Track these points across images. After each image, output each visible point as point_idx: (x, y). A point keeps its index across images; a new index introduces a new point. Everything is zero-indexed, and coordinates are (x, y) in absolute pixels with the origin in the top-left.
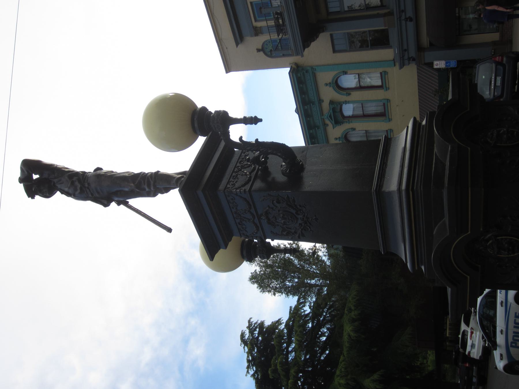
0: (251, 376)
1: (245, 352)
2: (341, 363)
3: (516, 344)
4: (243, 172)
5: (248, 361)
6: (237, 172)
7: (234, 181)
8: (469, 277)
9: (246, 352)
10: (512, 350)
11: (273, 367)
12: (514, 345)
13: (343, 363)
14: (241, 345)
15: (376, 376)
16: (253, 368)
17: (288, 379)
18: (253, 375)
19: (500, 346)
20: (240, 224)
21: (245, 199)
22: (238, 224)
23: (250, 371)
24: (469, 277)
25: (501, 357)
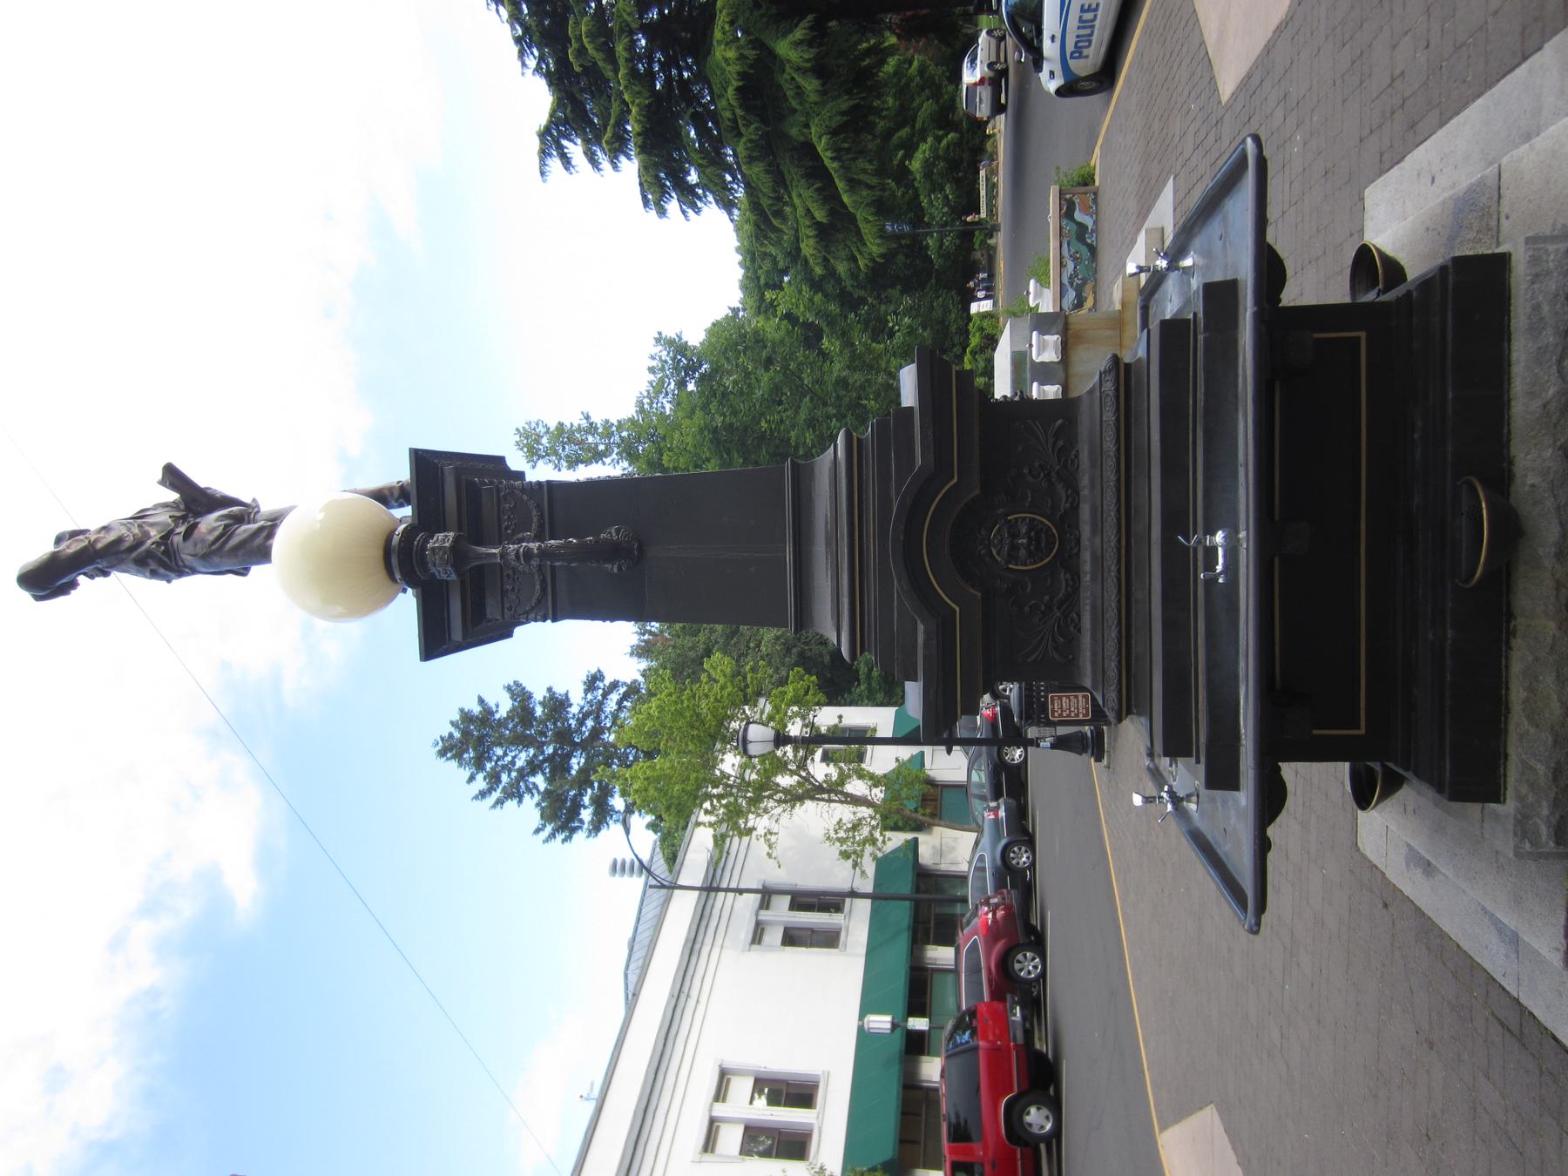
0: (533, 74)
1: (503, 22)
2: (721, 12)
3: (1081, 53)
5: (518, 40)
9: (505, 20)
10: (1071, 63)
11: (575, 45)
12: (1077, 55)
13: (724, 12)
14: (488, 8)
15: (798, 34)
16: (532, 53)
17: (616, 71)
18: (538, 70)
19: (1048, 60)
23: (527, 62)
25: (1028, 1025)
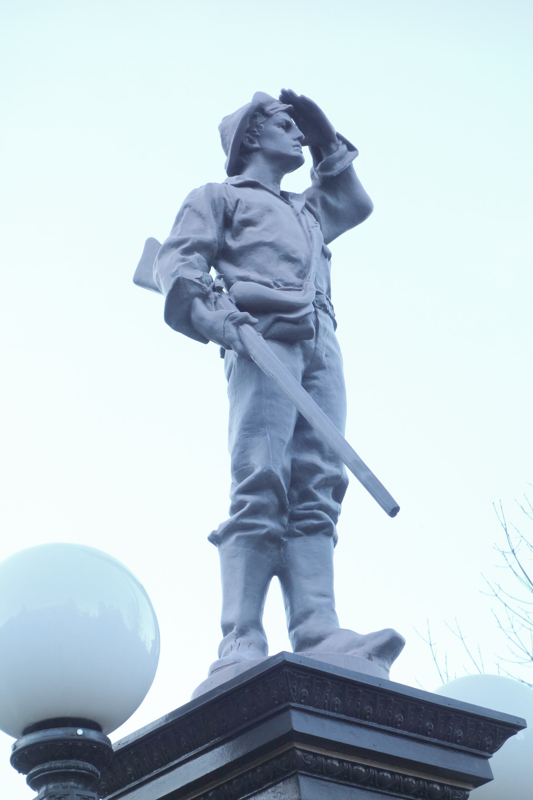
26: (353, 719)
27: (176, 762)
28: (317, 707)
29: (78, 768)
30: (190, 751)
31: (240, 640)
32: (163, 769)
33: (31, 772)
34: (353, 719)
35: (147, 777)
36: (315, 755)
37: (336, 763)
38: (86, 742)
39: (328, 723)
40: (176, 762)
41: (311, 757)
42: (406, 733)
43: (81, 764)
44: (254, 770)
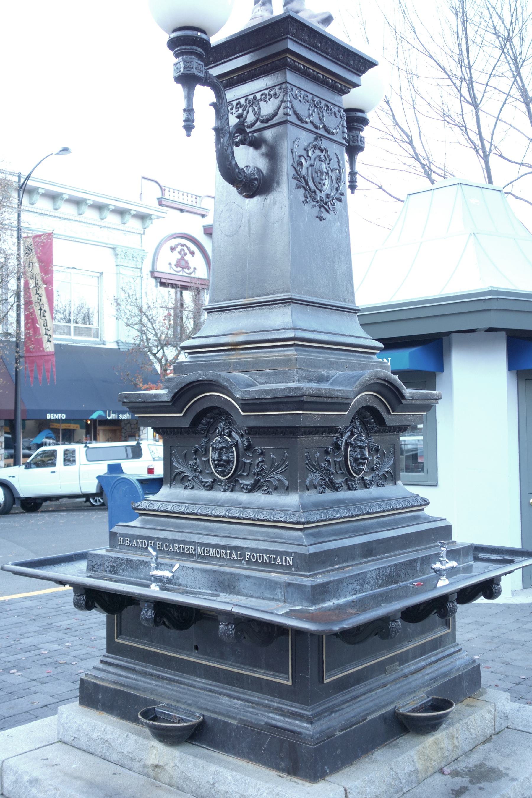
4: (314, 111)
6: (313, 101)
7: (301, 96)
8: (182, 415)
20: (237, 104)
21: (275, 114)
22: (238, 101)
24: (182, 415)
26: (312, 48)
27: (233, 57)
28: (299, 40)
29: (197, 50)
30: (240, 53)
31: (262, 7)
32: (226, 60)
33: (176, 49)
34: (312, 48)
35: (219, 63)
36: (295, 61)
37: (302, 66)
38: (202, 39)
39: (302, 48)
40: (233, 57)
41: (293, 62)
42: (331, 58)
43: (198, 49)
44: (267, 65)
